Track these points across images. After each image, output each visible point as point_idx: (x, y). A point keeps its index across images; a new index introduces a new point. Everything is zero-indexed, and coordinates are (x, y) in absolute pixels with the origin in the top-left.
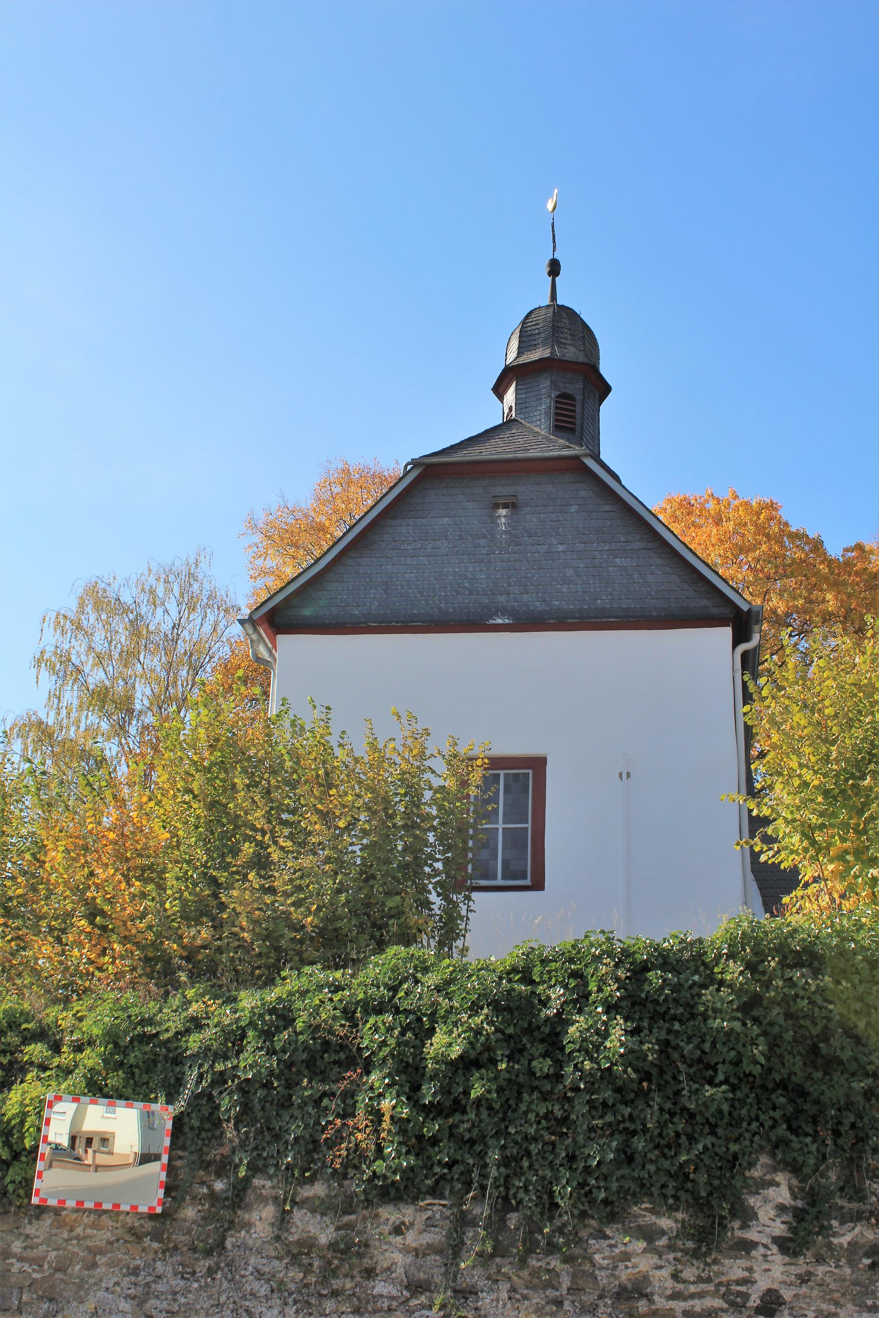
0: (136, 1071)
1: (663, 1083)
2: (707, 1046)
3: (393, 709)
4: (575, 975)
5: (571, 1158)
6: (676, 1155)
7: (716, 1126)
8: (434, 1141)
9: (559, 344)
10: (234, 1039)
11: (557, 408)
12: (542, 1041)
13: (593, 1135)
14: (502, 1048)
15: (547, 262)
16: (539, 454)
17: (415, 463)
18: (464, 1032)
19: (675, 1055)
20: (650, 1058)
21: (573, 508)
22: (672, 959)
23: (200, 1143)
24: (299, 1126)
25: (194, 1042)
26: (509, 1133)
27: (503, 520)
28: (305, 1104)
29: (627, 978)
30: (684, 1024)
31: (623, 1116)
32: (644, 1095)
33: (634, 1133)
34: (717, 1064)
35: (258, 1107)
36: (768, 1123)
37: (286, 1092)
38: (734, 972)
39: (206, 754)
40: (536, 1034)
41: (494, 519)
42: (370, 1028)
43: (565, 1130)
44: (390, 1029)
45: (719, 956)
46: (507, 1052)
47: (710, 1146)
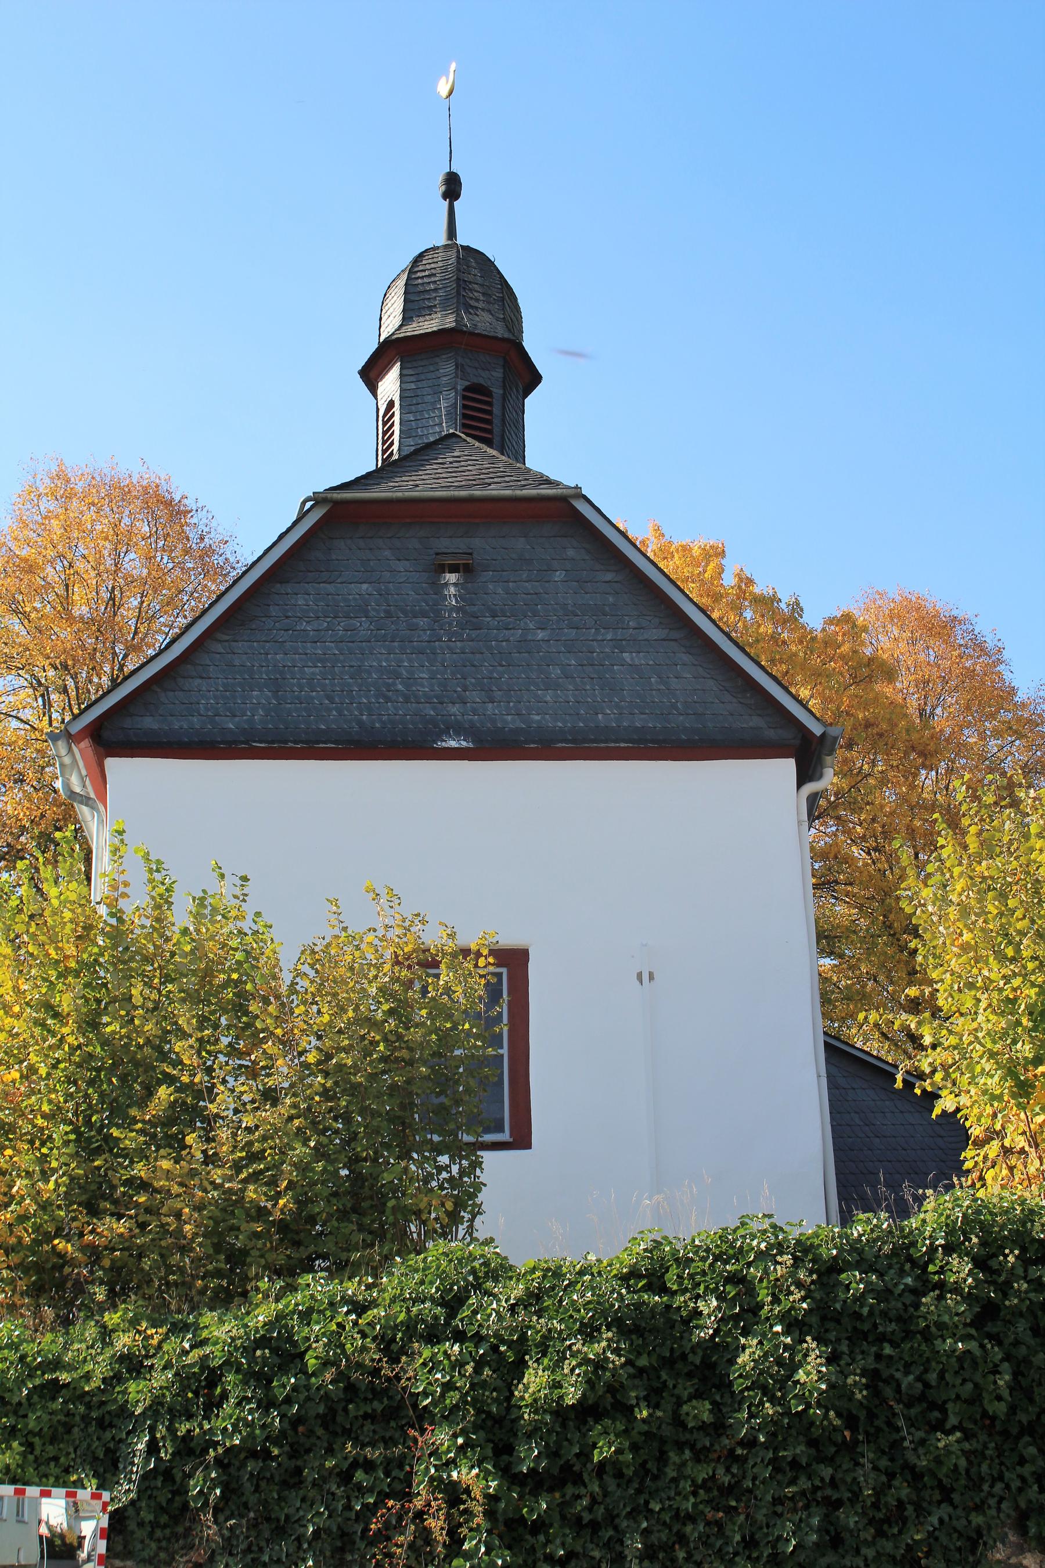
0: (37, 1440)
1: (872, 1430)
2: (932, 1377)
3: (368, 883)
4: (734, 1279)
5: (750, 1543)
6: (900, 1532)
7: (953, 1490)
8: (539, 1526)
9: (468, 307)
10: (203, 1386)
11: (464, 407)
12: (689, 1375)
13: (779, 1509)
14: (635, 1387)
15: (440, 178)
16: (508, 492)
17: (318, 499)
18: (579, 1365)
19: (888, 1392)
20: (859, 1396)
21: (559, 576)
22: (869, 1253)
23: (154, 1545)
24: (319, 1514)
25: (138, 1393)
26: (651, 1511)
27: (452, 590)
28: (324, 1479)
29: (813, 1282)
30: (898, 1346)
31: (822, 1480)
32: (850, 1448)
33: (838, 1504)
34: (945, 1402)
35: (248, 1487)
36: (1016, 1484)
37: (293, 1463)
38: (961, 1270)
39: (71, 950)
40: (679, 1365)
41: (439, 588)
42: (424, 1364)
43: (733, 1503)
44: (461, 1364)
45: (932, 1249)
46: (643, 1394)
47: (946, 1518)
